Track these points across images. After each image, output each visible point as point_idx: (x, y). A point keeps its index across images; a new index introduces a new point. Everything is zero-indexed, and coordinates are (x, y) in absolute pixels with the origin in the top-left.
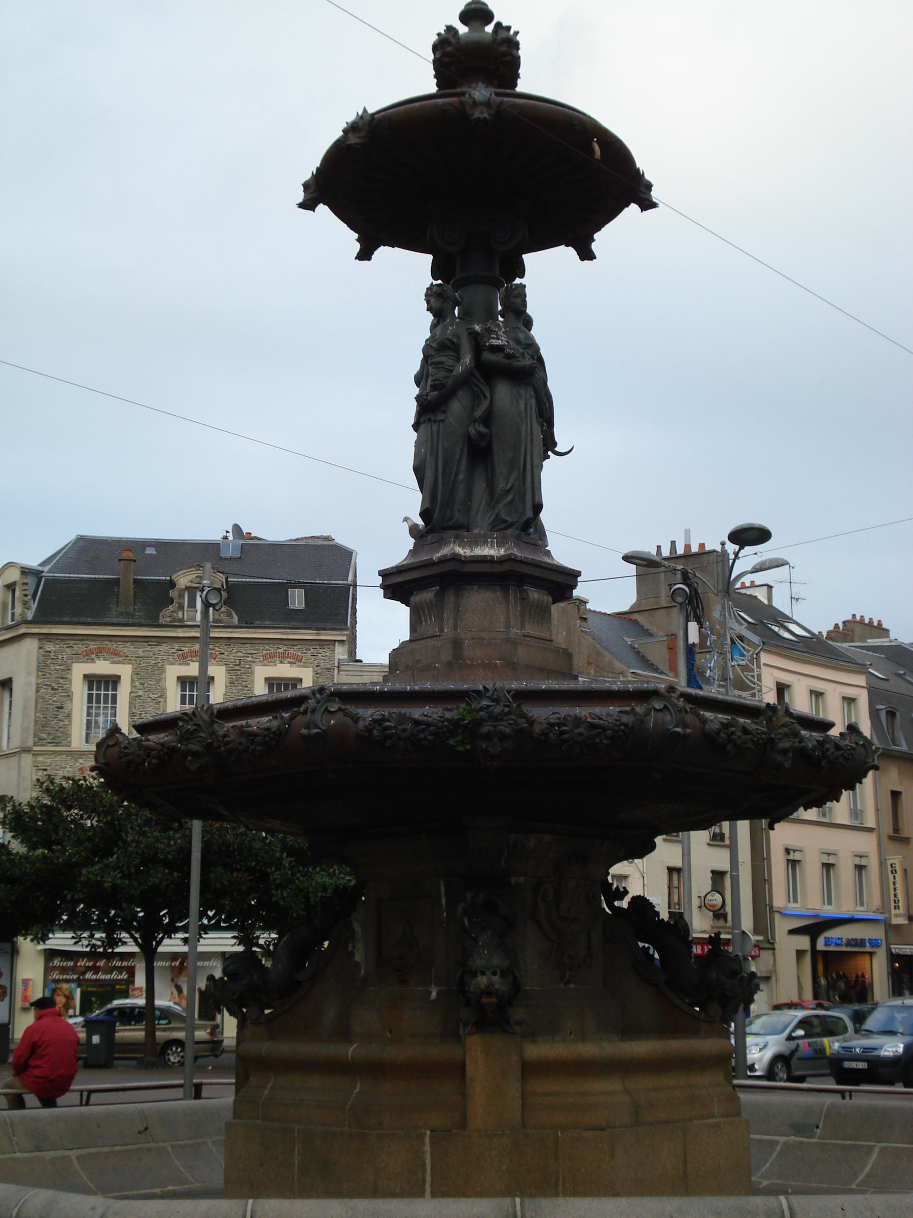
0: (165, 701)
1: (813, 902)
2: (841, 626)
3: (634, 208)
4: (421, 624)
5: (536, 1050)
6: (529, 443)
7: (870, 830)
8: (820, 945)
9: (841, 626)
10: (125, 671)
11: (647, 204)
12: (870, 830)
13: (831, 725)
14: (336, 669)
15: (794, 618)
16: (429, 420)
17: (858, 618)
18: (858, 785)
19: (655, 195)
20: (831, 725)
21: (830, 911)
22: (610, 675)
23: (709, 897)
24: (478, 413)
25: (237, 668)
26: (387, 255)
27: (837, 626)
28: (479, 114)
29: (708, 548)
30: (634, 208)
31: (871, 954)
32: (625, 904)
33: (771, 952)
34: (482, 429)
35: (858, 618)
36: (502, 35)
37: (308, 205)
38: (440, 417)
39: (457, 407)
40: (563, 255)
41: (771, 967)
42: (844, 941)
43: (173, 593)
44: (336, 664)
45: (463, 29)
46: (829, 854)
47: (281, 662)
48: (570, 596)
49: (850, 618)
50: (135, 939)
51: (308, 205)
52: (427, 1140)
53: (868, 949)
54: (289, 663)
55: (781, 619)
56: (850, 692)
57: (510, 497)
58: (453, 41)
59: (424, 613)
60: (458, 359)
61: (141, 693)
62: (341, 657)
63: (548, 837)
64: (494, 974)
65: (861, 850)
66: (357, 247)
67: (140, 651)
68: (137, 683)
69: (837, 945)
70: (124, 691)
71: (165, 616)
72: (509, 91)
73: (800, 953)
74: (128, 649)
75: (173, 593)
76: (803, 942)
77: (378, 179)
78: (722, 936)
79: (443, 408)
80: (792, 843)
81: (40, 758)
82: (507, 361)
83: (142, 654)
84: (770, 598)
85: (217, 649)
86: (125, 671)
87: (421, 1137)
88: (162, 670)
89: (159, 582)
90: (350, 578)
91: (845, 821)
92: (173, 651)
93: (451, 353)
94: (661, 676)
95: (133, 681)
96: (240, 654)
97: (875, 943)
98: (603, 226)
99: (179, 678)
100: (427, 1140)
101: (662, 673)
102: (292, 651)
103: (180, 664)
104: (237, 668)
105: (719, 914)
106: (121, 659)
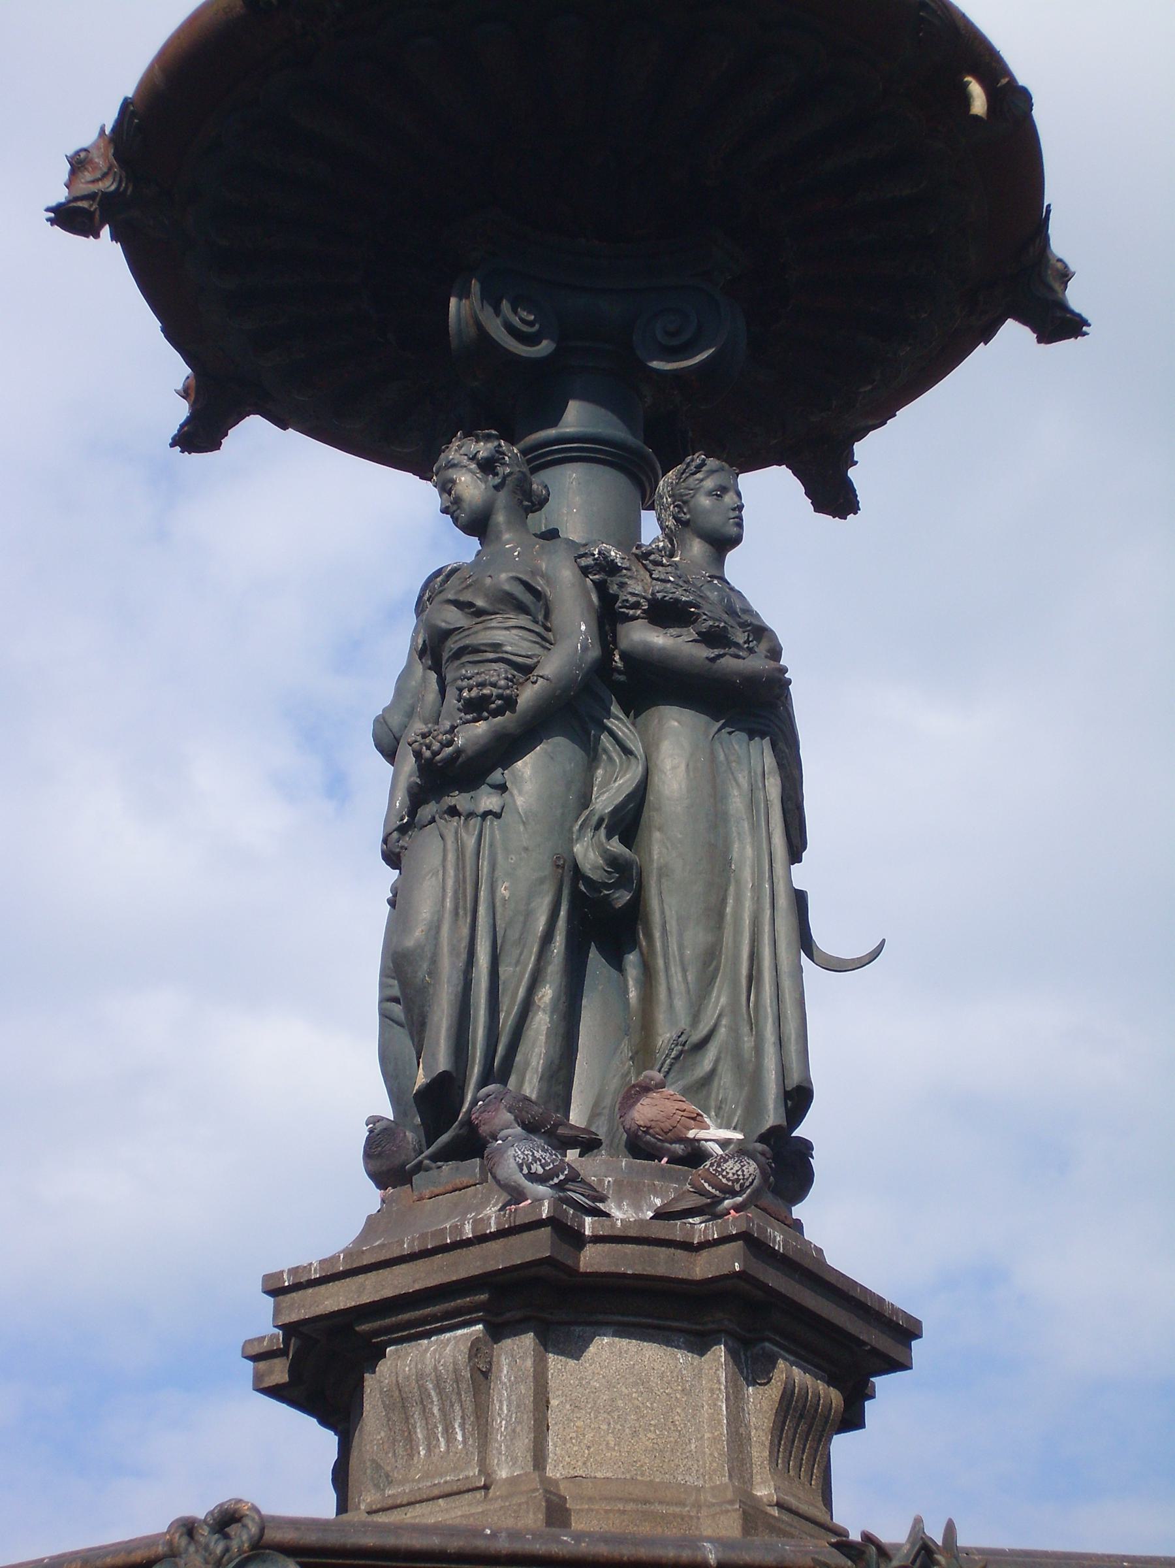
3: (1014, 335)
4: (412, 1452)
6: (767, 905)
11: (1056, 323)
16: (453, 811)
19: (1076, 297)
24: (605, 800)
30: (1014, 335)
37: (172, 445)
38: (488, 800)
48: (547, 1351)
51: (172, 445)
59: (426, 1413)
60: (545, 638)
72: (552, 432)
79: (496, 776)
81: (492, 1215)
82: (704, 652)
93: (523, 620)
98: (1038, 223)
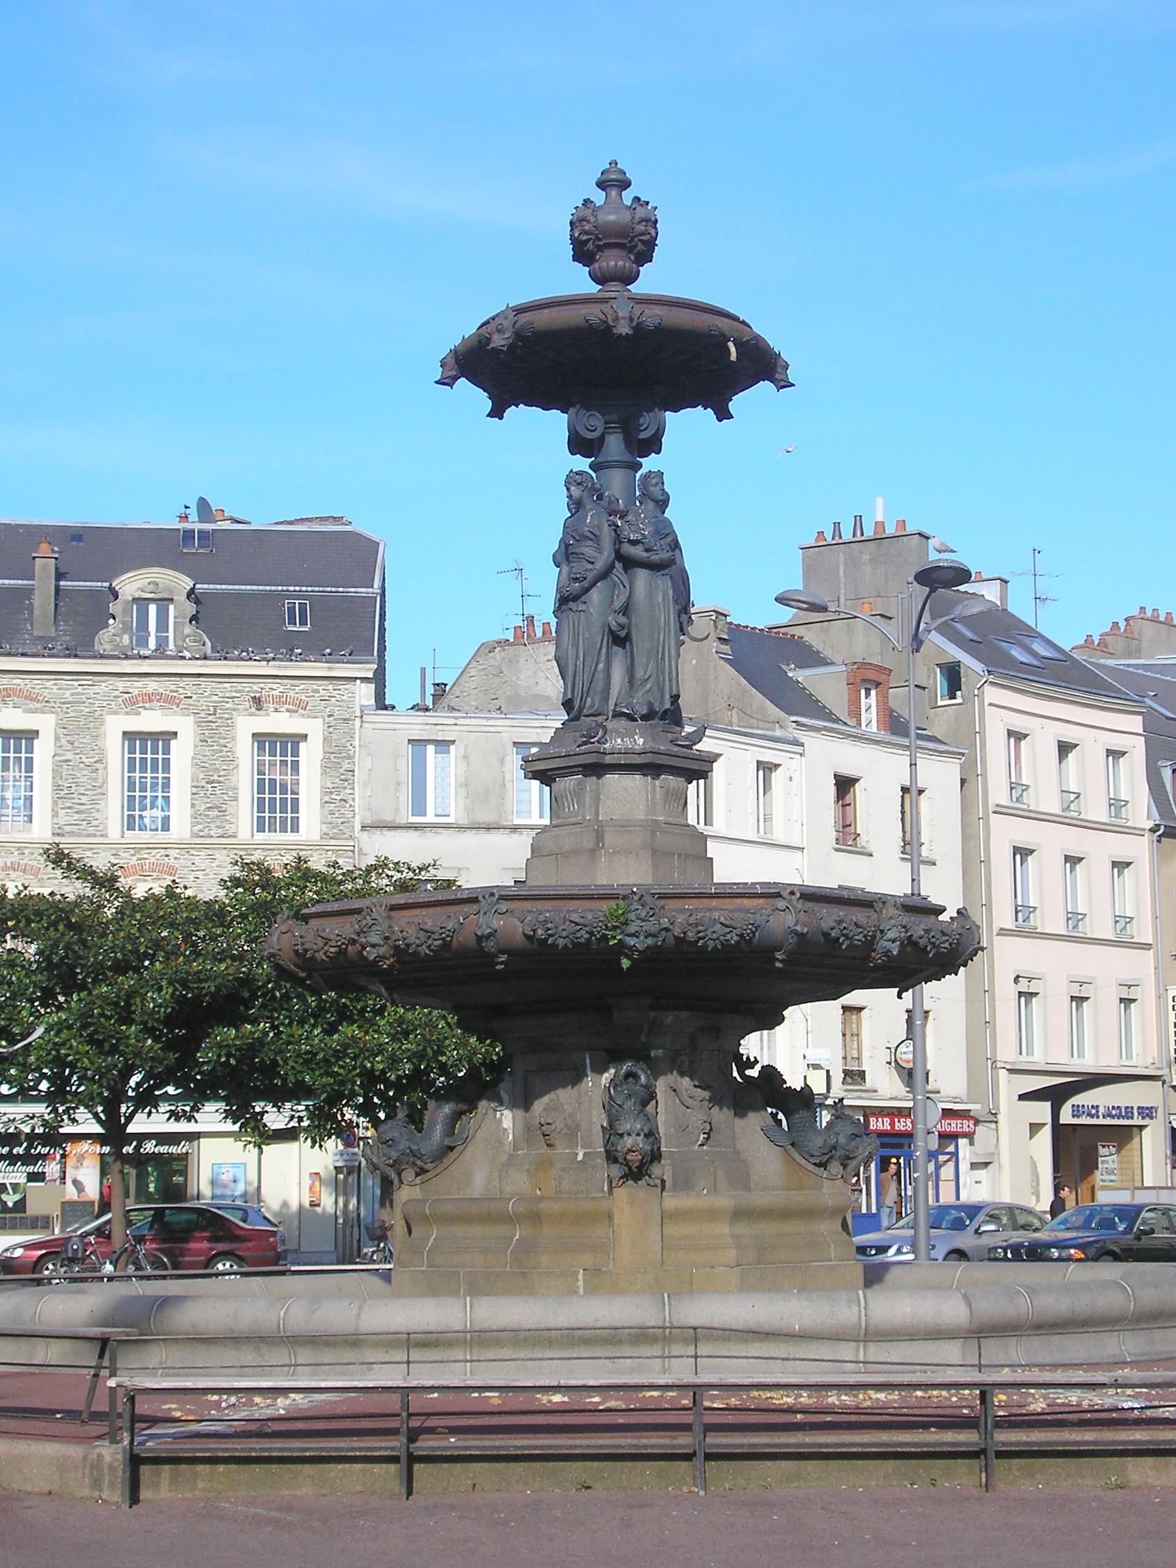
0: (106, 768)
1: (1054, 1051)
2: (1122, 625)
5: (672, 1202)
7: (1146, 947)
8: (1066, 1117)
9: (1122, 625)
10: (45, 724)
12: (1146, 947)
13: (942, 910)
14: (358, 721)
15: (1039, 629)
17: (1149, 613)
18: (962, 968)
19: (792, 375)
20: (942, 910)
21: (1089, 1063)
22: (761, 724)
23: (902, 1048)
24: (618, 604)
25: (210, 718)
26: (521, 415)
27: (1115, 624)
28: (623, 329)
29: (910, 529)
31: (1141, 1128)
32: (754, 1073)
33: (994, 1125)
34: (622, 619)
35: (1149, 613)
36: (640, 213)
39: (596, 596)
40: (701, 416)
41: (992, 1150)
42: (1101, 1110)
43: (114, 608)
44: (358, 714)
45: (599, 197)
46: (1082, 984)
47: (276, 710)
49: (1136, 612)
50: (96, 1116)
52: (580, 1277)
53: (1137, 1121)
54: (288, 710)
55: (1021, 632)
56: (1117, 742)
57: (648, 686)
58: (592, 219)
61: (69, 756)
62: (365, 703)
63: (685, 1014)
64: (638, 1135)
65: (1127, 976)
66: (489, 404)
67: (68, 693)
68: (63, 742)
69: (1090, 1115)
70: (43, 751)
71: (105, 639)
73: (1035, 1128)
74: (49, 688)
75: (114, 608)
76: (1043, 1110)
77: (513, 364)
78: (846, 1102)
80: (1025, 968)
82: (645, 554)
83: (70, 699)
84: (1004, 597)
85: (181, 690)
86: (45, 724)
87: (576, 1274)
88: (100, 721)
89: (92, 592)
90: (377, 583)
91: (1110, 936)
92: (117, 693)
93: (591, 543)
94: (835, 726)
95: (57, 738)
96: (215, 698)
97: (1147, 1112)
99: (125, 733)
100: (580, 1277)
101: (838, 720)
102: (292, 693)
103: (127, 713)
104: (210, 718)
105: (908, 1076)
106: (39, 705)
